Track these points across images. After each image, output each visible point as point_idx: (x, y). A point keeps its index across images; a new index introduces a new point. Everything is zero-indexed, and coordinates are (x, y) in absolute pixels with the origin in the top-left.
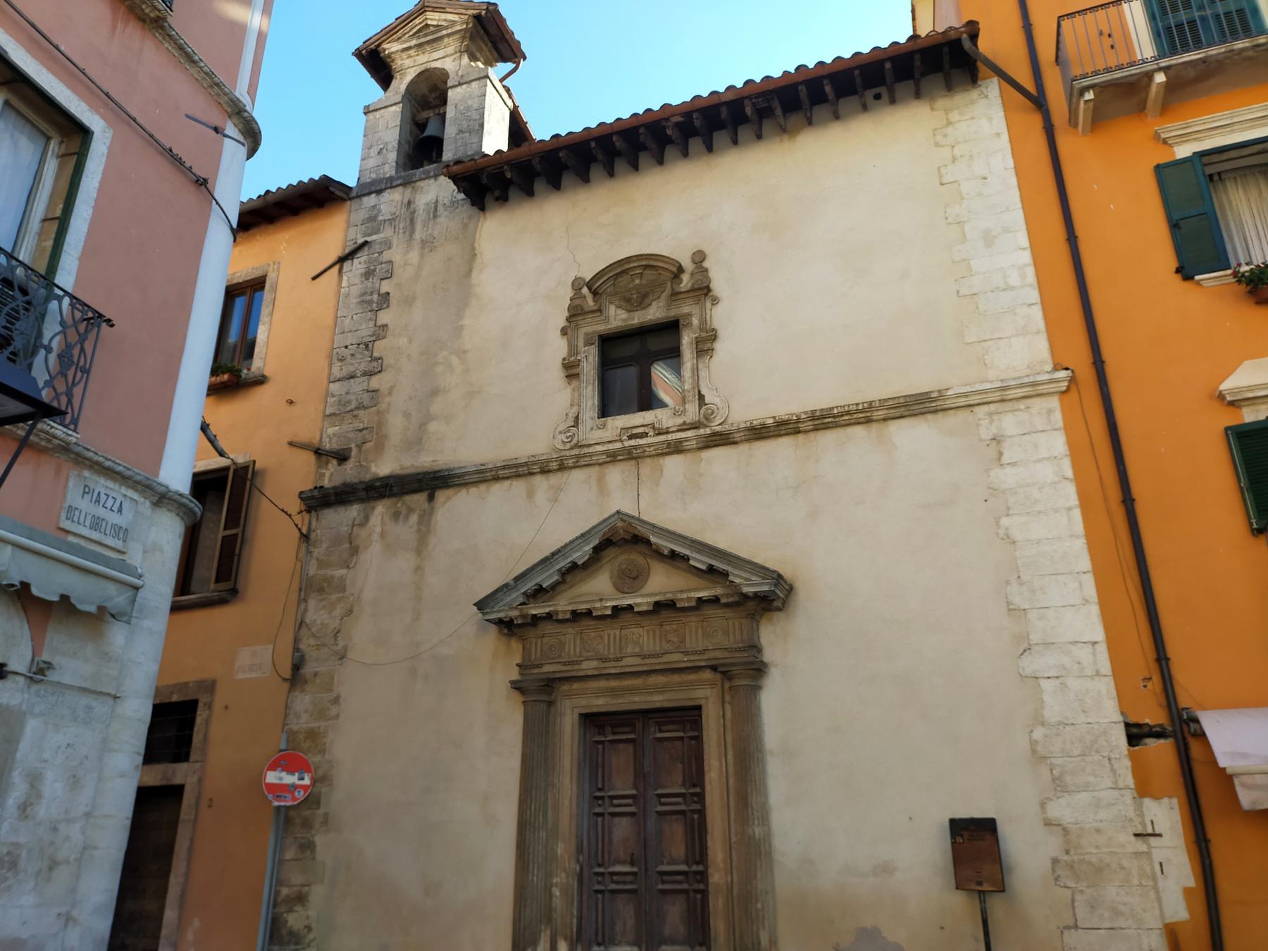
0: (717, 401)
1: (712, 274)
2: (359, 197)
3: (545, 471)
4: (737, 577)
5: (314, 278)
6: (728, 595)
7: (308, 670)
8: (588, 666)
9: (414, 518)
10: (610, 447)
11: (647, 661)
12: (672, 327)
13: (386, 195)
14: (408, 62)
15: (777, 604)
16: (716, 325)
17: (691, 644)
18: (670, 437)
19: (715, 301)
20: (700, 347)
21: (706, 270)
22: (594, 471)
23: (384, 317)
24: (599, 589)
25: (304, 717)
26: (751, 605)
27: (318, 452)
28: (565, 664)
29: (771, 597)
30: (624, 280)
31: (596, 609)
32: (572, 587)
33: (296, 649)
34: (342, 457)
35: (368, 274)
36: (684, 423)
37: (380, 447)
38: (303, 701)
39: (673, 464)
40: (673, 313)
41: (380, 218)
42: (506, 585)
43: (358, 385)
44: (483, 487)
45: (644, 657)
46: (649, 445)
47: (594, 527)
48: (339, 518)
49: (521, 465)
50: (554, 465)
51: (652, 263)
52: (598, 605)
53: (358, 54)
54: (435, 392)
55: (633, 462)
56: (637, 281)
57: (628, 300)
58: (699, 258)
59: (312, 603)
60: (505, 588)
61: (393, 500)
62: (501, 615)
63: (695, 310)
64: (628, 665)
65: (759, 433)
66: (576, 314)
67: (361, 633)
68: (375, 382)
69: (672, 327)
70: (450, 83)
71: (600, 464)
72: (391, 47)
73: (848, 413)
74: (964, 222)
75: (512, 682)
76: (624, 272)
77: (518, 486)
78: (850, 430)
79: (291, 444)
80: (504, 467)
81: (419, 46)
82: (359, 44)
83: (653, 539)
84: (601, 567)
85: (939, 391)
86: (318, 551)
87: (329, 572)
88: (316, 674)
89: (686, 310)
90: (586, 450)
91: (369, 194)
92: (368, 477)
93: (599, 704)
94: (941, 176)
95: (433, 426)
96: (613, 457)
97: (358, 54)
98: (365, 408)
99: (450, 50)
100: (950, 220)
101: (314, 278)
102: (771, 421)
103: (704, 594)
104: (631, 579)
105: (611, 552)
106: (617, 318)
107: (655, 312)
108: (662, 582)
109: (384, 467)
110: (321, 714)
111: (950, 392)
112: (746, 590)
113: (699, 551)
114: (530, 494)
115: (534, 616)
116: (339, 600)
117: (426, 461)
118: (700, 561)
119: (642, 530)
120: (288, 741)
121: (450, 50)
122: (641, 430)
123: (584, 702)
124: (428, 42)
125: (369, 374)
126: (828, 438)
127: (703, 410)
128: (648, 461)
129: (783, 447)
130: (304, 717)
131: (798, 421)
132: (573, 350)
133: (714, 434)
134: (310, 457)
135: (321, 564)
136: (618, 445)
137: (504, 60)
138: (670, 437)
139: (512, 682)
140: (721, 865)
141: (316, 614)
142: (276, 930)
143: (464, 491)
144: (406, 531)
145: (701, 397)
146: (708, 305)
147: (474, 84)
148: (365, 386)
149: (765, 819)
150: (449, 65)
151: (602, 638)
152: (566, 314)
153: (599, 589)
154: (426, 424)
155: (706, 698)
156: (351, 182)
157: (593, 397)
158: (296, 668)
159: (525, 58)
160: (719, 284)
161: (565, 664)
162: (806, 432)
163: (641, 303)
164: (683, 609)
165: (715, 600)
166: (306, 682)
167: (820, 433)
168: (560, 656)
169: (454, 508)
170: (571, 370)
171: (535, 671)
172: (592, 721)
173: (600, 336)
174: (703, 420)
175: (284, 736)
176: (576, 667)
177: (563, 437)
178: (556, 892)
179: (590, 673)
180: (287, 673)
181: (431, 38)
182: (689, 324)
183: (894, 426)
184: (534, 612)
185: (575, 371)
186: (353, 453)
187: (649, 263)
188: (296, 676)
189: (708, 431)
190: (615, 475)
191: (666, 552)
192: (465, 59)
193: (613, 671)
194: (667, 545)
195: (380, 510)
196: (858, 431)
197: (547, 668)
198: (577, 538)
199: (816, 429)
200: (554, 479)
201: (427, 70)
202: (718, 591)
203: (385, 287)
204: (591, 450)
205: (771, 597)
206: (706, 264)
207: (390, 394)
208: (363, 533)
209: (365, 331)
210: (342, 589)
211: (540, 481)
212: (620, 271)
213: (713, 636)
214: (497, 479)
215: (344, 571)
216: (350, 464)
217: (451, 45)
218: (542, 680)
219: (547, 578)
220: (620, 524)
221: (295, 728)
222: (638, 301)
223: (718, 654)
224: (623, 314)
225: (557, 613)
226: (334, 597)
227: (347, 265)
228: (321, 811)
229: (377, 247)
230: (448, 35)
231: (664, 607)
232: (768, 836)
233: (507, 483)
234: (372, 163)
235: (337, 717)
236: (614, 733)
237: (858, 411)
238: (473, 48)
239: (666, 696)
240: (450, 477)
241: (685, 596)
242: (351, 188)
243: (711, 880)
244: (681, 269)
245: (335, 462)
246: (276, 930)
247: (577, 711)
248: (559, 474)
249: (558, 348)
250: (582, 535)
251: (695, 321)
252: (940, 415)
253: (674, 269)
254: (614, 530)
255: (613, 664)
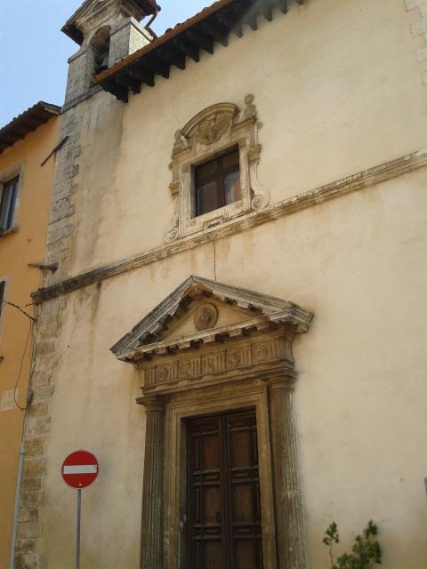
0: (262, 192)
1: (258, 108)
2: (64, 112)
3: (160, 259)
4: (267, 310)
5: (42, 165)
6: (261, 324)
7: (35, 402)
8: (182, 385)
9: (90, 299)
10: (196, 235)
11: (218, 377)
12: (234, 151)
13: (78, 107)
14: (91, 27)
15: (302, 327)
16: (260, 142)
17: (246, 361)
18: (231, 222)
19: (260, 126)
20: (251, 158)
21: (254, 106)
22: (188, 254)
23: (77, 180)
24: (188, 331)
25: (33, 431)
26: (281, 330)
27: (42, 268)
28: (169, 384)
29: (290, 327)
30: (204, 126)
31: (180, 344)
32: (171, 332)
33: (30, 390)
34: (53, 269)
35: (69, 155)
36: (242, 212)
37: (73, 260)
38: (32, 422)
39: (236, 241)
40: (234, 140)
41: (75, 121)
42: (128, 335)
43: (62, 224)
44: (126, 275)
45: (215, 375)
46: (219, 230)
47: (178, 288)
48: (51, 306)
49: (146, 257)
50: (164, 254)
51: (219, 109)
52: (181, 341)
53: (65, 30)
54: (100, 220)
55: (211, 244)
56: (213, 124)
57: (207, 138)
58: (249, 99)
59: (38, 360)
60: (128, 337)
61: (79, 291)
62: (126, 355)
63: (248, 135)
64: (200, 385)
65: (289, 209)
66: (177, 153)
67: (62, 376)
68: (71, 220)
69: (234, 151)
70: (111, 33)
71: (192, 249)
72: (81, 21)
73: (347, 183)
74: (423, 33)
75: (137, 400)
76: (204, 119)
77: (146, 271)
78: (350, 196)
79: (29, 265)
80: (136, 260)
81: (95, 16)
82: (64, 24)
83: (214, 292)
84: (187, 318)
85: (410, 155)
86: (43, 328)
87: (46, 340)
88: (39, 404)
89: (242, 136)
90: (182, 240)
91: (69, 109)
92: (66, 279)
93: (192, 410)
94: (406, 6)
95: (100, 242)
96: (198, 242)
97: (65, 30)
98: (66, 237)
99: (112, 14)
100: (414, 34)
101: (42, 165)
102: (295, 199)
103: (246, 325)
104: (208, 321)
105: (193, 305)
106: (202, 151)
107: (223, 142)
108: (228, 321)
109: (76, 271)
110: (41, 429)
111: (418, 154)
112: (272, 319)
113: (242, 296)
114: (152, 275)
115: (145, 353)
116: (52, 357)
117: (96, 263)
118: (244, 303)
119: (208, 287)
120: (25, 448)
121: (112, 14)
122: (215, 221)
123: (183, 410)
124: (100, 12)
125: (68, 216)
126: (336, 205)
127: (253, 201)
128: (221, 241)
129: (304, 218)
130: (33, 431)
131: (314, 195)
132: (176, 177)
133: (259, 215)
134: (38, 272)
135: (44, 336)
136: (201, 233)
137: (148, 14)
138: (231, 222)
139: (137, 400)
140: (269, 520)
141: (40, 367)
142: (19, 562)
143: (116, 279)
144: (85, 308)
145: (252, 192)
146: (255, 129)
147: (124, 30)
148: (65, 224)
149: (295, 484)
150: (111, 23)
151: (190, 364)
152: (171, 154)
153: (188, 331)
154: (97, 239)
155: (258, 400)
156: (60, 102)
157: (187, 206)
158: (30, 402)
159: (159, 9)
160: (262, 116)
161: (169, 384)
162: (320, 203)
163: (215, 137)
164: (234, 338)
165: (254, 329)
166: (34, 410)
167: (331, 202)
168: (165, 380)
169: (112, 289)
170: (174, 191)
171: (152, 391)
172: (189, 423)
173: (192, 166)
174: (253, 207)
175: (22, 444)
176: (175, 386)
177: (170, 235)
178: (167, 541)
179: (183, 389)
180: (24, 405)
181: (101, 10)
182: (245, 145)
183: (381, 188)
184: (144, 351)
185: (176, 191)
186: (60, 266)
187: (217, 109)
188: (29, 407)
189: (255, 214)
190: (201, 255)
191: (223, 299)
192: (121, 16)
193: (197, 387)
194: (223, 295)
195: (74, 296)
196: (356, 196)
197: (157, 389)
198: (168, 298)
199: (327, 199)
200: (165, 263)
201: (100, 29)
202: (255, 322)
203: (77, 162)
204: (185, 239)
205: (290, 327)
206: (253, 103)
207: (78, 225)
208: (64, 313)
209: (66, 192)
210: (53, 350)
211: (158, 267)
212: (201, 119)
213: (262, 352)
214: (134, 268)
215: (55, 339)
216: (58, 271)
217: (112, 10)
218: (153, 397)
219: (153, 328)
220: (194, 284)
221: (28, 439)
222: (213, 136)
223: (262, 368)
224: (204, 148)
225: (158, 350)
226: (49, 355)
227: (58, 153)
228: (41, 491)
229: (73, 139)
230: (110, 4)
231: (221, 338)
232: (298, 498)
233: (139, 270)
234: (72, 90)
235: (49, 431)
236: (206, 431)
237: (354, 181)
238: (126, 9)
239: (233, 401)
240: (108, 271)
241: (233, 328)
242: (60, 108)
243: (263, 531)
244: (237, 111)
245: (50, 272)
246: (19, 562)
247: (179, 417)
248: (169, 259)
249: (167, 177)
250: (171, 295)
251: (248, 142)
252: (414, 173)
253: (233, 110)
254: (191, 289)
255: (196, 382)
